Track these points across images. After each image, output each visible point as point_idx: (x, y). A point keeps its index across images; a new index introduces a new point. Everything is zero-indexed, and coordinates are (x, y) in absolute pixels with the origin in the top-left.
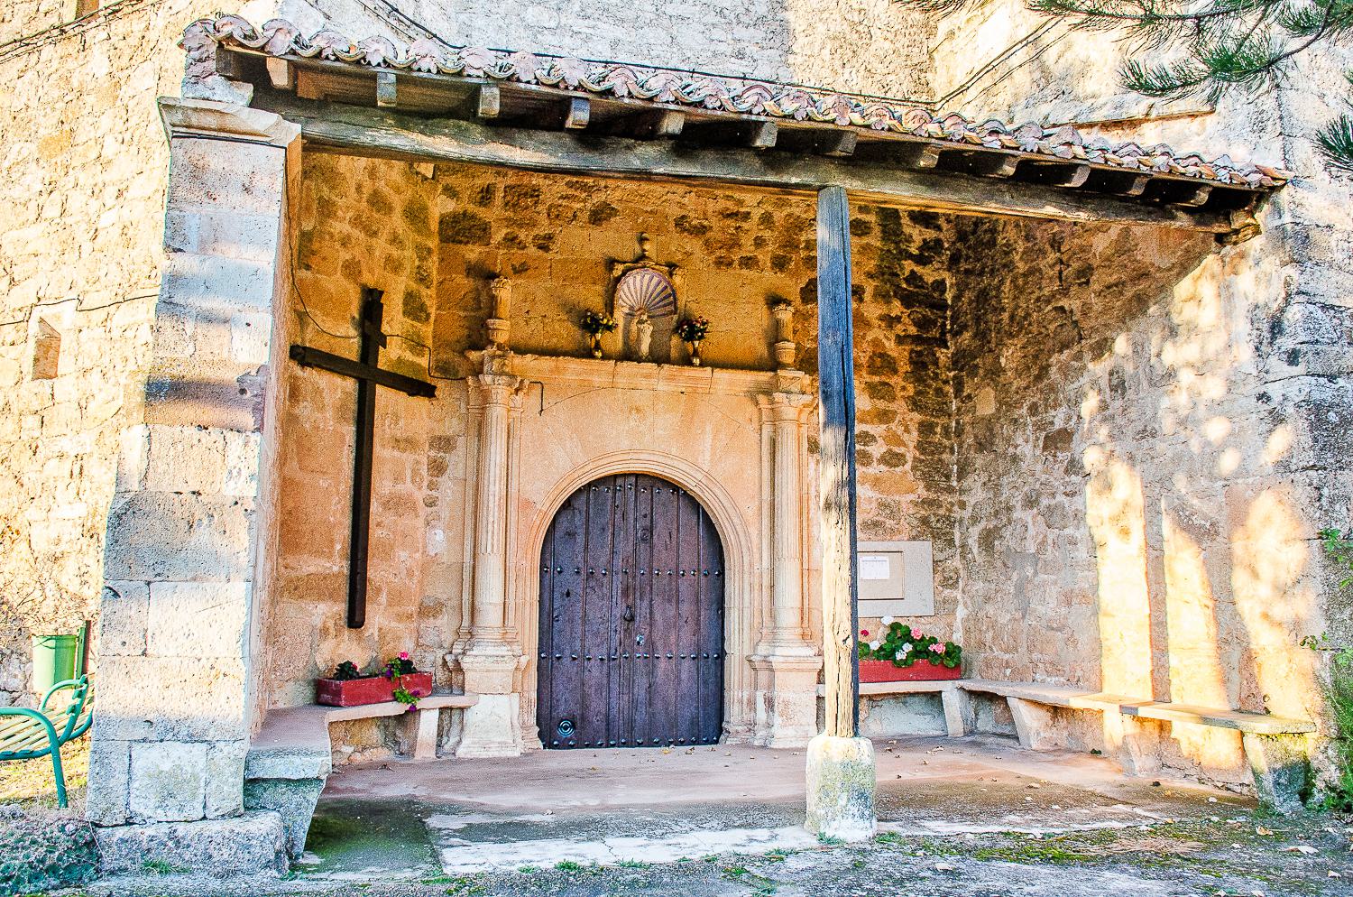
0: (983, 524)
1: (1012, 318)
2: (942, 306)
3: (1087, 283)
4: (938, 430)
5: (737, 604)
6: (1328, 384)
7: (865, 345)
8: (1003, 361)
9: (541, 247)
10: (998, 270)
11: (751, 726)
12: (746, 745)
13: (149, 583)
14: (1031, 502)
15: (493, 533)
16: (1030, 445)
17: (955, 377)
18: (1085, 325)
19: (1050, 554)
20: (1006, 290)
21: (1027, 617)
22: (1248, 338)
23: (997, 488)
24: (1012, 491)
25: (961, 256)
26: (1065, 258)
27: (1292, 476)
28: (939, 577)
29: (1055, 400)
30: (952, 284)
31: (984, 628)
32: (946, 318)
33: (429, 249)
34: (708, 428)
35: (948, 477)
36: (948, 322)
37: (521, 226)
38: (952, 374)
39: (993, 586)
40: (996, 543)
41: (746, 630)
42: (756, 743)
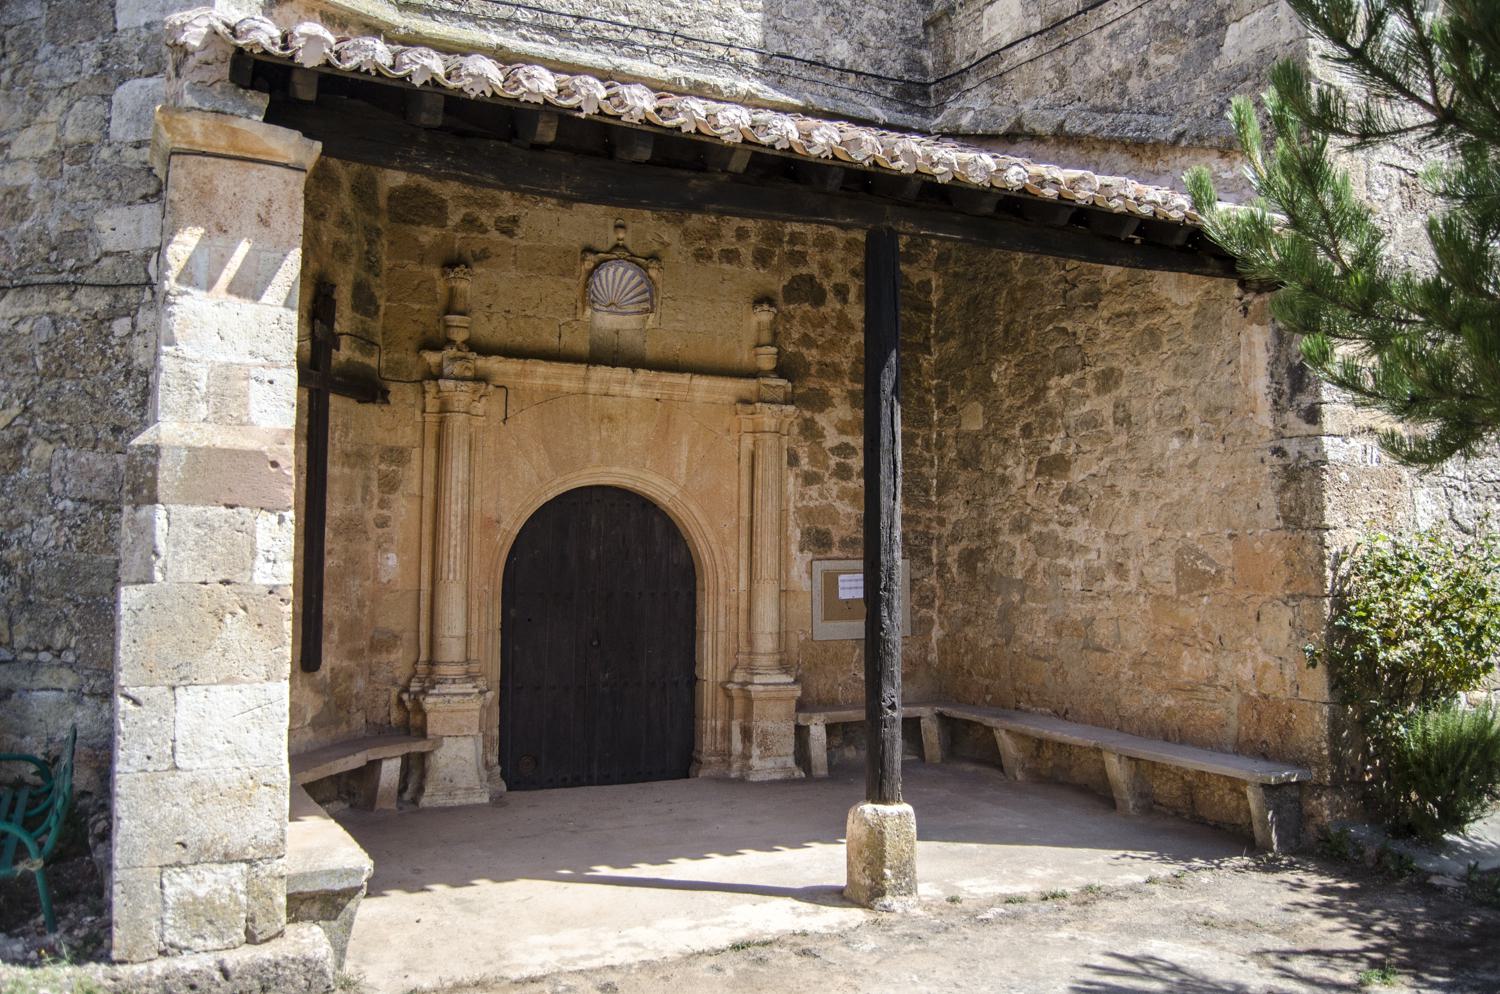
0: (964, 543)
1: (1007, 331)
2: (929, 309)
3: (1095, 307)
4: (919, 441)
5: (710, 627)
6: (1342, 444)
7: (848, 350)
8: (994, 376)
9: (503, 232)
10: (993, 278)
11: (726, 755)
12: (723, 780)
13: (174, 688)
14: (1019, 527)
15: (455, 558)
16: (1021, 469)
17: (938, 386)
18: (1091, 351)
19: (1039, 580)
20: (1002, 301)
21: (1012, 643)
22: (1267, 391)
23: (982, 509)
24: (1000, 514)
25: (949, 257)
26: (1069, 277)
27: (1303, 534)
28: (915, 596)
29: (1052, 425)
30: (938, 286)
31: (962, 651)
32: (930, 322)
33: (379, 229)
34: (685, 439)
35: (927, 492)
36: (932, 326)
37: (481, 206)
38: (935, 382)
39: (974, 609)
40: (979, 565)
41: (721, 655)
42: (733, 775)
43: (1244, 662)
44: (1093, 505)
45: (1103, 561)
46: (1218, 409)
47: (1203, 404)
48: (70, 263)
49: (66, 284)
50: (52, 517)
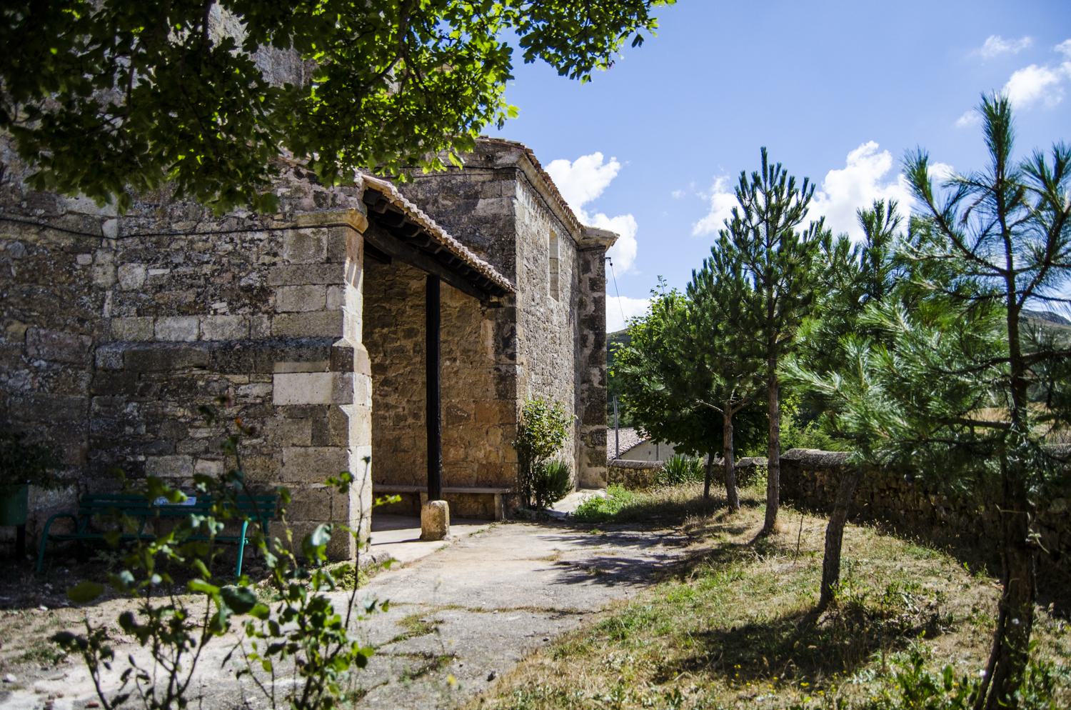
43: (480, 451)
44: (400, 388)
45: (406, 412)
46: (469, 351)
47: (462, 348)
48: (41, 212)
49: (37, 224)
50: (27, 371)
